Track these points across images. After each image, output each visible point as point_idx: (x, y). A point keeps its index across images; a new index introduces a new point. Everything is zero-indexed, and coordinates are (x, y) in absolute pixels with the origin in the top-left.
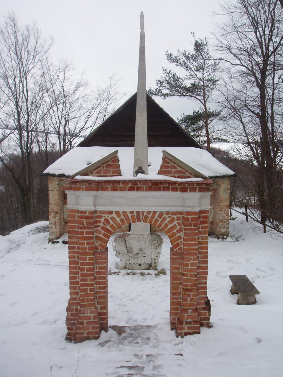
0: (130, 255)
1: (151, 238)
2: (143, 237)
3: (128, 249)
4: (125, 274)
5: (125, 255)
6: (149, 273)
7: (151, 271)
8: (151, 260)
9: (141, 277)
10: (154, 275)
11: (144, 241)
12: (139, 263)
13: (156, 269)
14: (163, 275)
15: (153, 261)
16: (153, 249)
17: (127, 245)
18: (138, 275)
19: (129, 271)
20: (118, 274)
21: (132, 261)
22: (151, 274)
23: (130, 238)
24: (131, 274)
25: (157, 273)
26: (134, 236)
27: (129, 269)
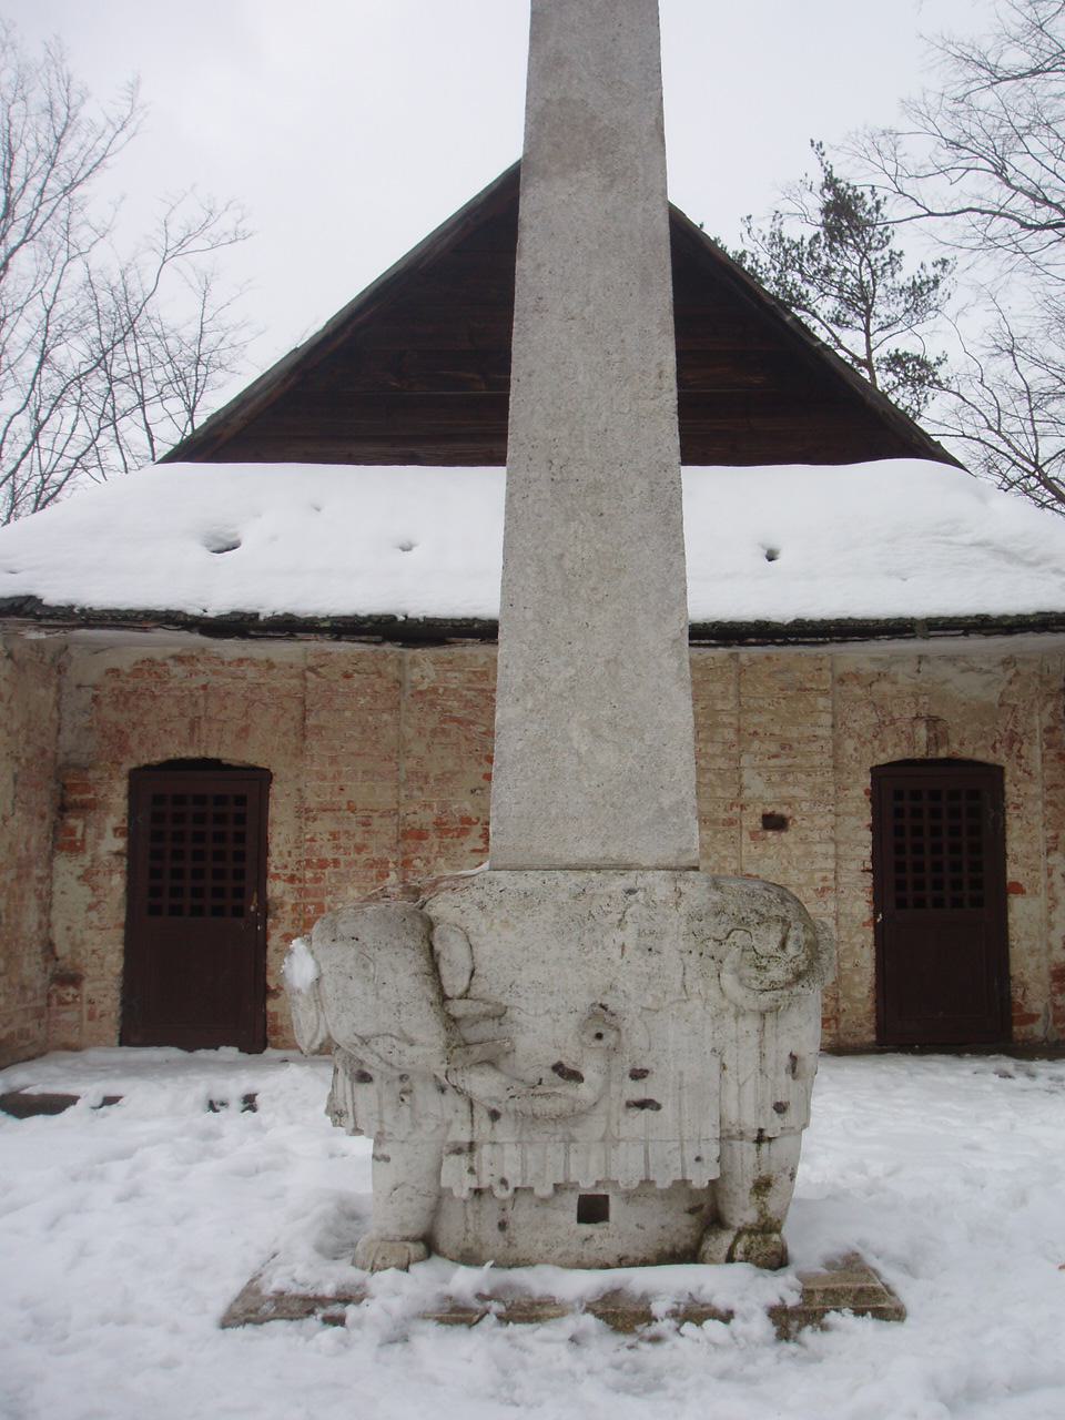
0: (483, 1084)
1: (716, 897)
2: (619, 884)
3: (452, 1022)
4: (424, 1316)
5: (426, 1097)
6: (704, 1296)
7: (713, 1280)
8: (715, 1150)
9: (606, 1348)
10: (761, 1327)
11: (631, 929)
12: (587, 1186)
13: (777, 1261)
14: (866, 1326)
15: (746, 1159)
16: (740, 1014)
17: (445, 970)
18: (571, 1324)
19: (465, 1281)
20: (335, 1309)
21: (506, 1158)
22: (727, 1317)
23: (478, 895)
24: (491, 1319)
25: (793, 1300)
26: (530, 881)
27: (470, 1259)
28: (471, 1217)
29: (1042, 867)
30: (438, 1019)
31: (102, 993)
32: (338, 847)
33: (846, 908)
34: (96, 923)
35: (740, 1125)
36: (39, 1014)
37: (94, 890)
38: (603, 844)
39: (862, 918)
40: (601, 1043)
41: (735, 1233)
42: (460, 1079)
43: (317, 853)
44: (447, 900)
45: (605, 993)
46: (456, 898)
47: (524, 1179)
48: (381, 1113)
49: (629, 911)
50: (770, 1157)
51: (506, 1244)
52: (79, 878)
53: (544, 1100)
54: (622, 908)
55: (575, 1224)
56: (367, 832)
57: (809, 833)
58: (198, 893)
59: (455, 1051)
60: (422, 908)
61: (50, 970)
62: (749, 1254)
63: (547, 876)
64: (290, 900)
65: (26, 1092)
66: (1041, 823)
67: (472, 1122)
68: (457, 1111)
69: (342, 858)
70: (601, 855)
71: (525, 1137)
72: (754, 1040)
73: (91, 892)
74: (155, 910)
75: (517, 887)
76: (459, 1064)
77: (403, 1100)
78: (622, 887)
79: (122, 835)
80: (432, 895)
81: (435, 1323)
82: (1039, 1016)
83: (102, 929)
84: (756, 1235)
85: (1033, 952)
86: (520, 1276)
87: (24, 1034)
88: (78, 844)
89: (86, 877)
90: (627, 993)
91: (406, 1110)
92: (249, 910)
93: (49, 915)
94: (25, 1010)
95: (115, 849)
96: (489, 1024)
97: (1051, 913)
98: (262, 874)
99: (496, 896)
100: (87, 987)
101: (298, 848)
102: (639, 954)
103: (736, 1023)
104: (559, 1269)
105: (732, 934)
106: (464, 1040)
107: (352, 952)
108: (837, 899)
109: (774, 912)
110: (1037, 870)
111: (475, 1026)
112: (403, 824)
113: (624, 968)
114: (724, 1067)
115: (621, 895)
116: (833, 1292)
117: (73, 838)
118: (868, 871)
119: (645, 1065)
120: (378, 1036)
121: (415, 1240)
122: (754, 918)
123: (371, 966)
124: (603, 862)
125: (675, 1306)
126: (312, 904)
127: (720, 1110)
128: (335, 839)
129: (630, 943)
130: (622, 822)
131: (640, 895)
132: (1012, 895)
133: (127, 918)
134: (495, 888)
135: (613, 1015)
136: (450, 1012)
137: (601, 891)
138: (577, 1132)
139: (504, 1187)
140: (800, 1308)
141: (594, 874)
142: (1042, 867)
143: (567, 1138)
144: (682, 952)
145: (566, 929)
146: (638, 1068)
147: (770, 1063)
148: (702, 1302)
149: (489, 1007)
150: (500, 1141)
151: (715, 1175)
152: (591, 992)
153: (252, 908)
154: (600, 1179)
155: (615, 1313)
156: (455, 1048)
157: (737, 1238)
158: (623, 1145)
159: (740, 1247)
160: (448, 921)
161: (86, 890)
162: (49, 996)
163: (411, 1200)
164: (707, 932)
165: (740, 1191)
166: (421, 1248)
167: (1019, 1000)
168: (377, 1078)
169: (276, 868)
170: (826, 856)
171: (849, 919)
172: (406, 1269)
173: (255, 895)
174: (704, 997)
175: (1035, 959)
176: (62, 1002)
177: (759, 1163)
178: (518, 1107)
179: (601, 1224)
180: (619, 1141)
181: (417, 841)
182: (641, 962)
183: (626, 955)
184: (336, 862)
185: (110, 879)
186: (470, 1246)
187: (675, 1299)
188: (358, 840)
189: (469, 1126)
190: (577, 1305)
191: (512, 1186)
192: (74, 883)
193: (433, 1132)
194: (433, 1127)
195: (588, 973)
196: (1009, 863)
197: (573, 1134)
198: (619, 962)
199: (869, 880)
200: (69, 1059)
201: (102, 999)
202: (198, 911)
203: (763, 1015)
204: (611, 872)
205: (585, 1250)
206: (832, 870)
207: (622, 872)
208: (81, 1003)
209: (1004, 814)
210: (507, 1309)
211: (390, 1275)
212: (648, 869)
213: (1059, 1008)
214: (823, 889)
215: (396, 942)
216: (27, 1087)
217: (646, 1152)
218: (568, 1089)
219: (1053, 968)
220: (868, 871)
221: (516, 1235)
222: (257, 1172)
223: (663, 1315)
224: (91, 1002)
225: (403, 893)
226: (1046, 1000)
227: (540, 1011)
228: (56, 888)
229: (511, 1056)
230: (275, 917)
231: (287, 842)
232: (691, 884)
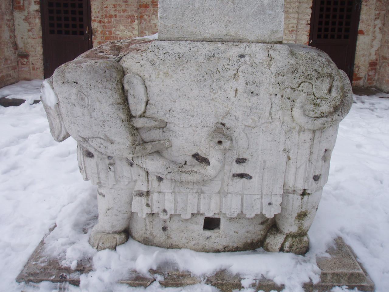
1: (293, 61)
2: (235, 51)
4: (121, 282)
5: (123, 169)
6: (270, 276)
8: (280, 200)
11: (242, 80)
16: (301, 130)
17: (131, 100)
23: (151, 56)
24: (156, 284)
26: (182, 48)
28: (148, 223)
29: (372, 25)
30: (127, 130)
31: (36, 61)
32: (116, 10)
33: (299, 38)
34: (32, 36)
35: (294, 188)
36: (14, 68)
37: (29, 24)
38: (226, 26)
39: (305, 41)
40: (221, 147)
41: (285, 236)
42: (140, 162)
43: (109, 12)
44: (132, 58)
45: (224, 117)
46: (137, 56)
47: (176, 210)
48: (98, 174)
49: (241, 69)
50: (308, 202)
51: (166, 237)
52: (24, 20)
53: (187, 175)
54: (236, 67)
56: (127, 5)
57: (289, 9)
58: (67, 26)
59: (137, 147)
60: (118, 61)
61: (17, 53)
62: (292, 247)
63: (193, 44)
64: (100, 30)
65: (7, 98)
66: (374, 8)
67: (148, 181)
68: (139, 175)
69: (118, 15)
70: (225, 32)
71: (177, 190)
72: (308, 145)
73: (29, 25)
74: (52, 32)
75: (174, 51)
76: (139, 155)
77: (110, 168)
78: (236, 53)
79: (38, 4)
80: (126, 53)
81: (128, 285)
82: (362, 78)
83: (34, 39)
84: (296, 238)
85: (364, 55)
86: (172, 255)
87: (8, 76)
88: (22, 7)
89: (26, 19)
90: (237, 117)
91: (111, 174)
92: (86, 33)
93: (14, 33)
94: (8, 67)
95: (36, 9)
96: (157, 131)
97: (372, 42)
98: (89, 20)
99: (161, 57)
100: (31, 59)
101: (102, 10)
102: (246, 95)
103: (299, 135)
104: (193, 252)
105: (302, 85)
106: (142, 139)
107: (74, 91)
108: (297, 34)
109: (326, 70)
110: (370, 26)
111: (149, 132)
112: (140, 2)
113: (236, 103)
114: (289, 159)
115: (235, 58)
116: (337, 275)
117: (20, 5)
118: (309, 24)
119: (245, 156)
120: (93, 138)
121: (119, 233)
122: (315, 74)
123: (86, 99)
124: (227, 37)
125: (254, 282)
126: (108, 31)
127: (284, 180)
128: (115, 7)
129: (241, 89)
130: (238, 13)
131: (247, 58)
132: (359, 35)
133: (42, 34)
134: (161, 52)
135: (228, 129)
136: (134, 125)
137: (224, 55)
138: (204, 189)
139: (165, 213)
140: (320, 284)
141: (220, 45)
142: (372, 25)
143: (199, 191)
144: (271, 95)
145: (203, 79)
146: (241, 157)
147: (315, 156)
148: (268, 279)
149: (156, 123)
150: (164, 191)
151: (278, 211)
152: (216, 116)
153: (87, 32)
154: (216, 212)
155: (222, 283)
156: (137, 145)
157: (286, 239)
158: (229, 195)
159: (287, 244)
160: (133, 71)
161: (27, 24)
162: (18, 62)
163: (117, 215)
164: (287, 83)
165: (290, 217)
166: (123, 236)
167: (356, 72)
168: (95, 156)
169: (94, 18)
170: (294, 18)
171: (300, 41)
172: (115, 249)
173: (87, 27)
174: (282, 121)
175: (364, 58)
176: (22, 64)
177: (302, 205)
178: (173, 178)
179: (216, 230)
180: (228, 193)
181: (145, 9)
182: (247, 100)
183: (238, 95)
184: (116, 16)
185: (35, 21)
186: (148, 236)
187: (255, 278)
188: (123, 7)
189: (146, 183)
190: (202, 279)
191: (169, 213)
192: (22, 21)
193: (127, 185)
194: (127, 183)
195: (215, 105)
196: (360, 22)
197: (203, 189)
198: (233, 99)
199: (309, 27)
200: (26, 84)
201: (37, 63)
202: (67, 33)
203: (314, 132)
204: (230, 44)
205: (207, 243)
206: (296, 24)
207: (237, 44)
208: (29, 64)
209: (361, 4)
210: (165, 279)
211: (104, 254)
212: (252, 42)
213: (370, 75)
214: (292, 31)
215: (100, 86)
216: (7, 96)
217: (242, 199)
218: (199, 168)
219: (370, 62)
220: (309, 24)
221: (171, 234)
222: (69, 154)
223: (248, 286)
224: (32, 64)
225: (111, 50)
226: (366, 72)
227: (186, 126)
228: (16, 23)
229: (169, 149)
230: (95, 36)
231: (98, 8)
232: (277, 52)
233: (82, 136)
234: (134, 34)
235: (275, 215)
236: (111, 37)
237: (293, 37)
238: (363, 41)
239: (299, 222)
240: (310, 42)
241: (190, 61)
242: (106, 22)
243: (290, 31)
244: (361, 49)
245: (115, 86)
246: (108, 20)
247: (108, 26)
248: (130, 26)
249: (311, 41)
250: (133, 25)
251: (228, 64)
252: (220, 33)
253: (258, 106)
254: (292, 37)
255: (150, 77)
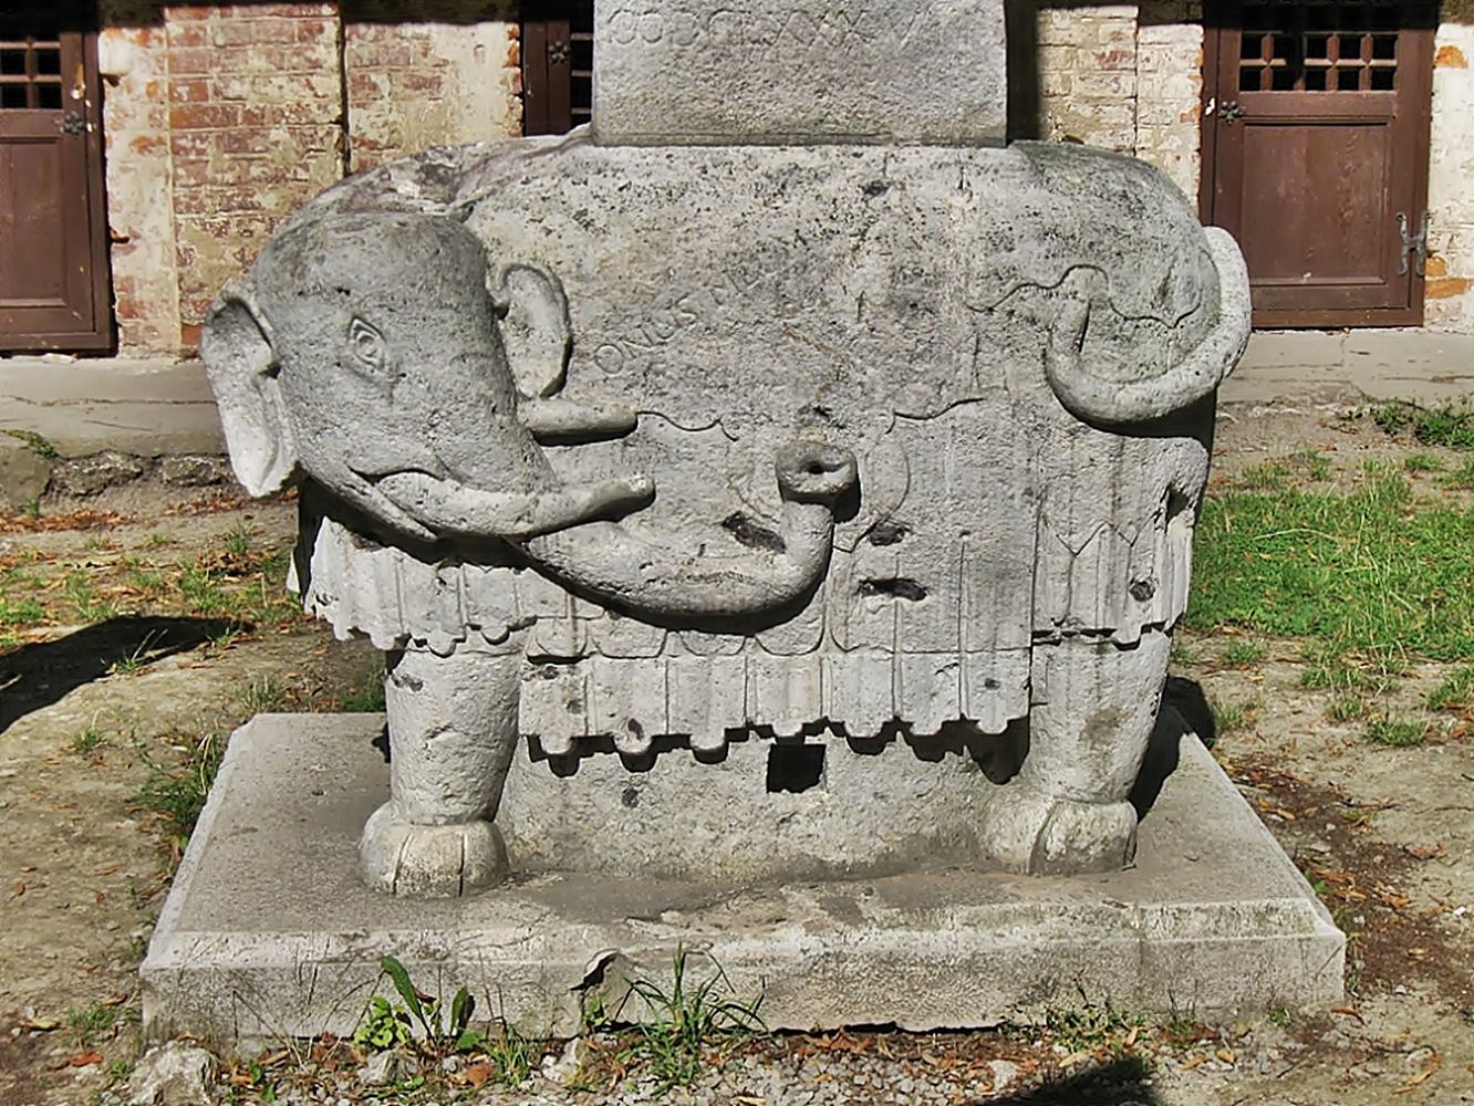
45: (827, 388)
55: (762, 796)
131: (893, 196)
156: (541, 493)
173: (81, 68)
198: (853, 329)
207: (856, 149)
214: (1114, 55)
233: (361, 470)
234: (320, 94)
235: (1010, 722)
236: (204, 111)
237: (1123, 84)
238: (1464, 102)
239: (1092, 748)
240: (1208, 111)
241: (708, 210)
242: (176, 39)
243: (1104, 55)
244: (1456, 141)
245: (467, 296)
246: (187, 29)
247: (188, 55)
248: (297, 53)
249: (1212, 102)
250: (313, 50)
251: (831, 217)
252: (801, 115)
253: (934, 349)
254: (1115, 86)
255: (579, 266)
